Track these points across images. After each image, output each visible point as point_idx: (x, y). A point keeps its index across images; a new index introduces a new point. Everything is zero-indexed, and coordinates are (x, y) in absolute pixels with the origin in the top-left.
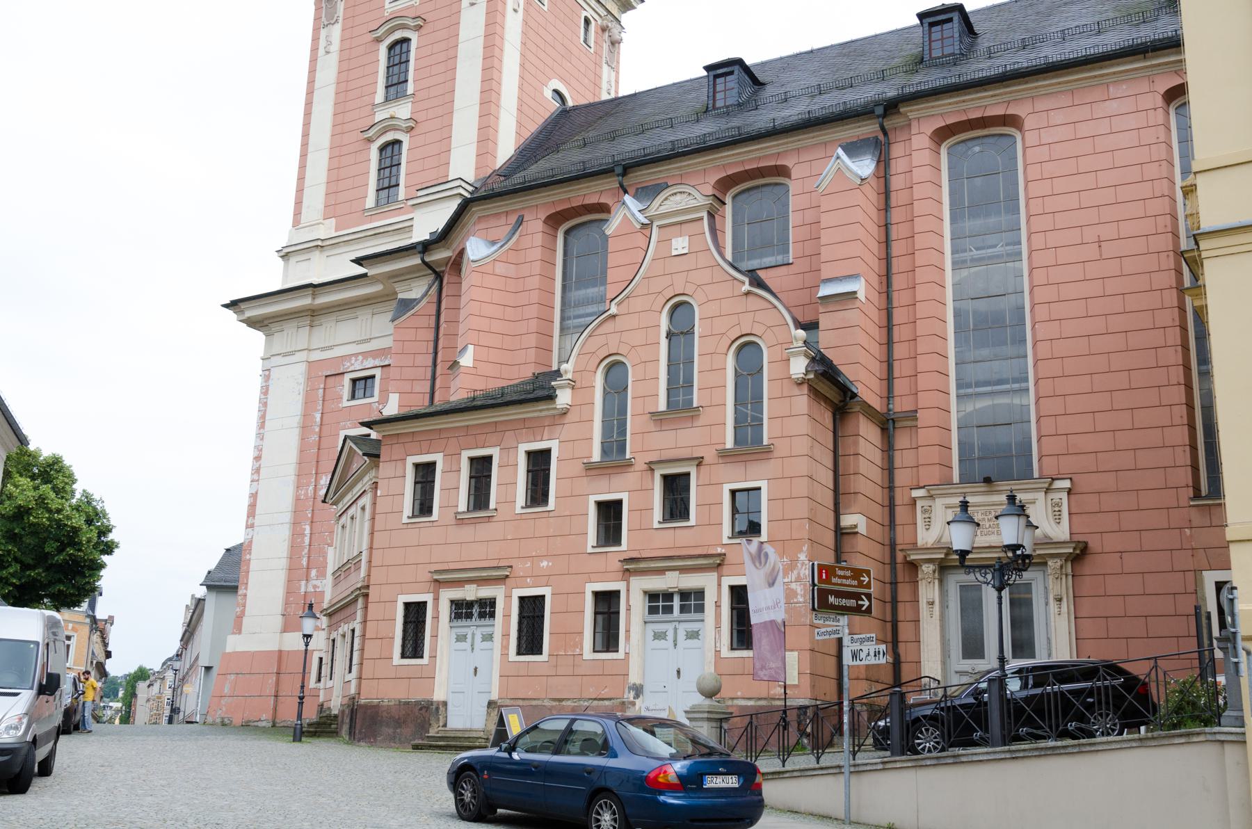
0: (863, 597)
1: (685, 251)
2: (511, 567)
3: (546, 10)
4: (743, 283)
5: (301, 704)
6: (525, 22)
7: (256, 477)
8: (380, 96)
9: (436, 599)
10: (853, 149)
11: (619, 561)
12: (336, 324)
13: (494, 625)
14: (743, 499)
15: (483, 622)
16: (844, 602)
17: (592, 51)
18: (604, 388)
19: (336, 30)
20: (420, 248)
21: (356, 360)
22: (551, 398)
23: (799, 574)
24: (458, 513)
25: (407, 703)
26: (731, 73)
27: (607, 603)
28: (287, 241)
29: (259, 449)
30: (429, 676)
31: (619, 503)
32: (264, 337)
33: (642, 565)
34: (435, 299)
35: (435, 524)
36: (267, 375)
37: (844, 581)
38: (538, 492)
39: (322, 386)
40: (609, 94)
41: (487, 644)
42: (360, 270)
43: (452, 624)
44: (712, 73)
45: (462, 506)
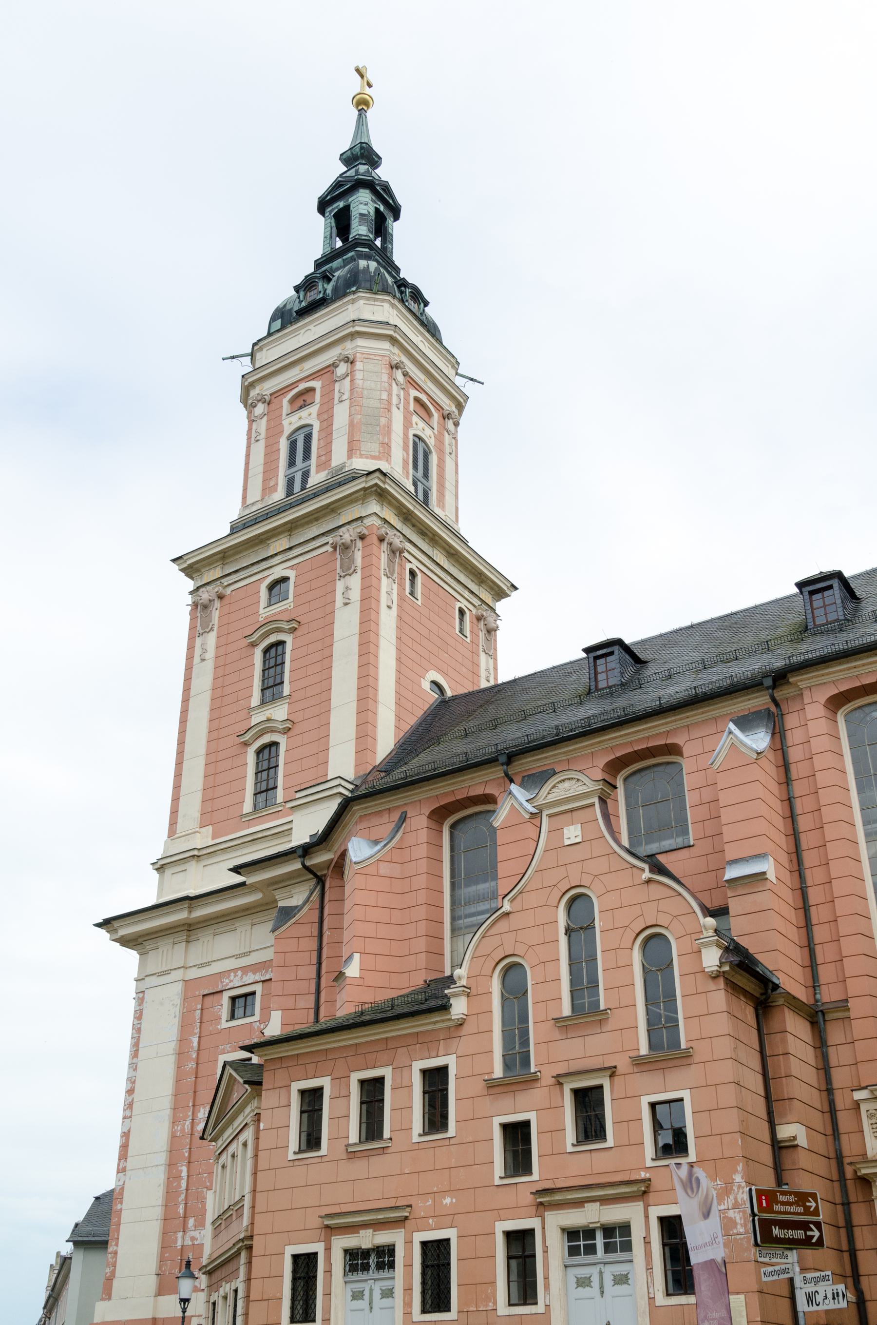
0: (812, 1226)
1: (579, 840)
3: (420, 604)
4: (643, 870)
8: (255, 700)
9: (328, 1249)
13: (393, 1278)
15: (382, 1274)
17: (468, 640)
20: (300, 852)
22: (445, 1008)
23: (736, 1199)
26: (612, 653)
29: (132, 1081)
31: (526, 1124)
32: (138, 956)
33: (558, 1197)
34: (317, 905)
39: (199, 1006)
40: (488, 681)
41: (387, 1302)
44: (592, 655)
45: (354, 1138)
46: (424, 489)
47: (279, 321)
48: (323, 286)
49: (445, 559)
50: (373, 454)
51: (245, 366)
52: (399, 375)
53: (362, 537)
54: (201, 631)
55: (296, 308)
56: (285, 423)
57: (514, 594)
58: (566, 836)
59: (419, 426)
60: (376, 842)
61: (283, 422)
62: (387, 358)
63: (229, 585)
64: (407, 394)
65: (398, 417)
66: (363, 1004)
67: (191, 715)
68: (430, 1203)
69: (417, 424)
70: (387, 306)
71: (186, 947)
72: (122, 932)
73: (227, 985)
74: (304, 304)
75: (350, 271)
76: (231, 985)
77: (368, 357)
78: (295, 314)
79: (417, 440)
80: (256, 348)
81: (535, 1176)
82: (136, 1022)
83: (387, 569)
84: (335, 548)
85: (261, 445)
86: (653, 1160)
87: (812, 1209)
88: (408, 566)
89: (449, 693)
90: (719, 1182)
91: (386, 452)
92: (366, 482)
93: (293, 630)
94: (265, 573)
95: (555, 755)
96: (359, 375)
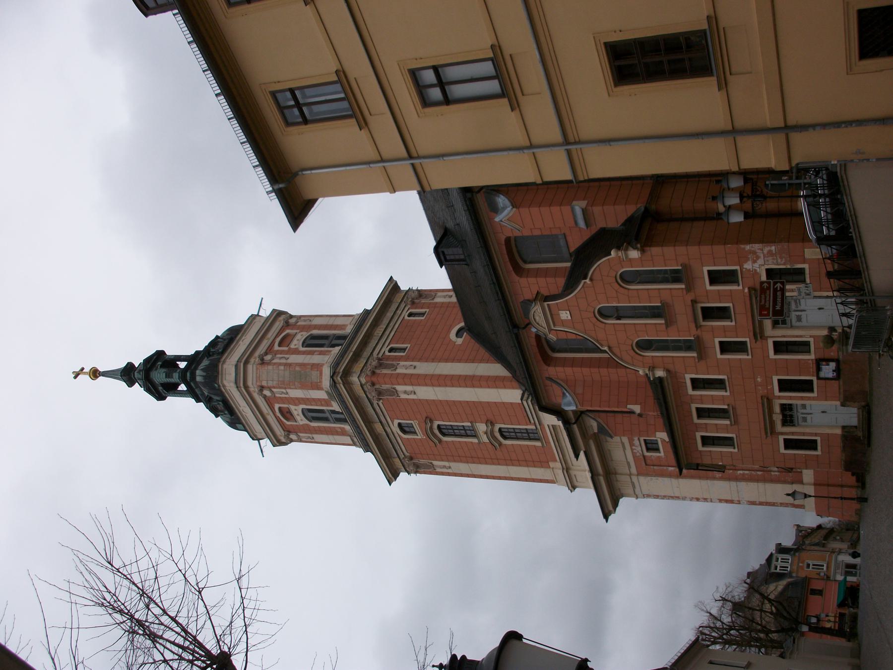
0: (775, 287)
1: (568, 312)
2: (762, 397)
3: (409, 345)
4: (585, 282)
5: (845, 499)
6: (420, 360)
7: (709, 500)
8: (475, 440)
9: (782, 434)
10: (495, 210)
11: (756, 342)
12: (608, 442)
13: (797, 405)
14: (716, 278)
15: (795, 409)
16: (779, 300)
17: (428, 310)
18: (638, 283)
19: (435, 463)
20: (567, 426)
21: (635, 450)
22: (660, 379)
23: (758, 249)
24: (731, 425)
25: (844, 447)
26: (443, 252)
27: (779, 347)
28: (564, 487)
29: (691, 499)
30: (827, 437)
31: (721, 343)
32: (624, 498)
33: (758, 331)
34: (597, 414)
35: (738, 435)
36: (649, 496)
37: (767, 299)
38: (718, 384)
39: (652, 467)
40: (451, 296)
41: (808, 407)
42: (582, 455)
43: (797, 425)
44: (444, 263)
45: (727, 422)
46: (335, 339)
47: (237, 425)
48: (215, 402)
49: (379, 327)
50: (319, 375)
51: (266, 442)
52: (268, 358)
53: (373, 384)
54: (433, 469)
55: (228, 416)
56: (301, 423)
57: (395, 278)
58: (566, 318)
59: (296, 343)
60: (564, 394)
61: (301, 424)
62: (258, 366)
63: (404, 454)
64: (278, 352)
65: (294, 359)
66: (654, 403)
67: (484, 473)
68: (760, 388)
69: (295, 345)
70: (225, 366)
71: (619, 474)
72: (611, 508)
73: (640, 453)
74: (226, 412)
75: (204, 387)
76: (641, 452)
77: (258, 378)
78: (233, 417)
79: (305, 345)
80: (255, 438)
81: (748, 340)
82: (660, 498)
83: (392, 369)
84: (380, 399)
85: (315, 436)
86: (739, 285)
87: (768, 285)
88: (387, 353)
89: (462, 324)
90: (750, 256)
91: (318, 367)
92: (339, 383)
93: (431, 421)
94: (396, 435)
95: (512, 302)
96: (270, 384)
